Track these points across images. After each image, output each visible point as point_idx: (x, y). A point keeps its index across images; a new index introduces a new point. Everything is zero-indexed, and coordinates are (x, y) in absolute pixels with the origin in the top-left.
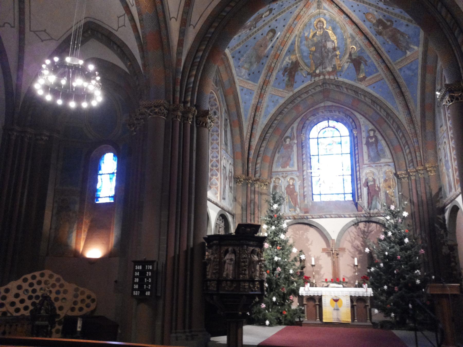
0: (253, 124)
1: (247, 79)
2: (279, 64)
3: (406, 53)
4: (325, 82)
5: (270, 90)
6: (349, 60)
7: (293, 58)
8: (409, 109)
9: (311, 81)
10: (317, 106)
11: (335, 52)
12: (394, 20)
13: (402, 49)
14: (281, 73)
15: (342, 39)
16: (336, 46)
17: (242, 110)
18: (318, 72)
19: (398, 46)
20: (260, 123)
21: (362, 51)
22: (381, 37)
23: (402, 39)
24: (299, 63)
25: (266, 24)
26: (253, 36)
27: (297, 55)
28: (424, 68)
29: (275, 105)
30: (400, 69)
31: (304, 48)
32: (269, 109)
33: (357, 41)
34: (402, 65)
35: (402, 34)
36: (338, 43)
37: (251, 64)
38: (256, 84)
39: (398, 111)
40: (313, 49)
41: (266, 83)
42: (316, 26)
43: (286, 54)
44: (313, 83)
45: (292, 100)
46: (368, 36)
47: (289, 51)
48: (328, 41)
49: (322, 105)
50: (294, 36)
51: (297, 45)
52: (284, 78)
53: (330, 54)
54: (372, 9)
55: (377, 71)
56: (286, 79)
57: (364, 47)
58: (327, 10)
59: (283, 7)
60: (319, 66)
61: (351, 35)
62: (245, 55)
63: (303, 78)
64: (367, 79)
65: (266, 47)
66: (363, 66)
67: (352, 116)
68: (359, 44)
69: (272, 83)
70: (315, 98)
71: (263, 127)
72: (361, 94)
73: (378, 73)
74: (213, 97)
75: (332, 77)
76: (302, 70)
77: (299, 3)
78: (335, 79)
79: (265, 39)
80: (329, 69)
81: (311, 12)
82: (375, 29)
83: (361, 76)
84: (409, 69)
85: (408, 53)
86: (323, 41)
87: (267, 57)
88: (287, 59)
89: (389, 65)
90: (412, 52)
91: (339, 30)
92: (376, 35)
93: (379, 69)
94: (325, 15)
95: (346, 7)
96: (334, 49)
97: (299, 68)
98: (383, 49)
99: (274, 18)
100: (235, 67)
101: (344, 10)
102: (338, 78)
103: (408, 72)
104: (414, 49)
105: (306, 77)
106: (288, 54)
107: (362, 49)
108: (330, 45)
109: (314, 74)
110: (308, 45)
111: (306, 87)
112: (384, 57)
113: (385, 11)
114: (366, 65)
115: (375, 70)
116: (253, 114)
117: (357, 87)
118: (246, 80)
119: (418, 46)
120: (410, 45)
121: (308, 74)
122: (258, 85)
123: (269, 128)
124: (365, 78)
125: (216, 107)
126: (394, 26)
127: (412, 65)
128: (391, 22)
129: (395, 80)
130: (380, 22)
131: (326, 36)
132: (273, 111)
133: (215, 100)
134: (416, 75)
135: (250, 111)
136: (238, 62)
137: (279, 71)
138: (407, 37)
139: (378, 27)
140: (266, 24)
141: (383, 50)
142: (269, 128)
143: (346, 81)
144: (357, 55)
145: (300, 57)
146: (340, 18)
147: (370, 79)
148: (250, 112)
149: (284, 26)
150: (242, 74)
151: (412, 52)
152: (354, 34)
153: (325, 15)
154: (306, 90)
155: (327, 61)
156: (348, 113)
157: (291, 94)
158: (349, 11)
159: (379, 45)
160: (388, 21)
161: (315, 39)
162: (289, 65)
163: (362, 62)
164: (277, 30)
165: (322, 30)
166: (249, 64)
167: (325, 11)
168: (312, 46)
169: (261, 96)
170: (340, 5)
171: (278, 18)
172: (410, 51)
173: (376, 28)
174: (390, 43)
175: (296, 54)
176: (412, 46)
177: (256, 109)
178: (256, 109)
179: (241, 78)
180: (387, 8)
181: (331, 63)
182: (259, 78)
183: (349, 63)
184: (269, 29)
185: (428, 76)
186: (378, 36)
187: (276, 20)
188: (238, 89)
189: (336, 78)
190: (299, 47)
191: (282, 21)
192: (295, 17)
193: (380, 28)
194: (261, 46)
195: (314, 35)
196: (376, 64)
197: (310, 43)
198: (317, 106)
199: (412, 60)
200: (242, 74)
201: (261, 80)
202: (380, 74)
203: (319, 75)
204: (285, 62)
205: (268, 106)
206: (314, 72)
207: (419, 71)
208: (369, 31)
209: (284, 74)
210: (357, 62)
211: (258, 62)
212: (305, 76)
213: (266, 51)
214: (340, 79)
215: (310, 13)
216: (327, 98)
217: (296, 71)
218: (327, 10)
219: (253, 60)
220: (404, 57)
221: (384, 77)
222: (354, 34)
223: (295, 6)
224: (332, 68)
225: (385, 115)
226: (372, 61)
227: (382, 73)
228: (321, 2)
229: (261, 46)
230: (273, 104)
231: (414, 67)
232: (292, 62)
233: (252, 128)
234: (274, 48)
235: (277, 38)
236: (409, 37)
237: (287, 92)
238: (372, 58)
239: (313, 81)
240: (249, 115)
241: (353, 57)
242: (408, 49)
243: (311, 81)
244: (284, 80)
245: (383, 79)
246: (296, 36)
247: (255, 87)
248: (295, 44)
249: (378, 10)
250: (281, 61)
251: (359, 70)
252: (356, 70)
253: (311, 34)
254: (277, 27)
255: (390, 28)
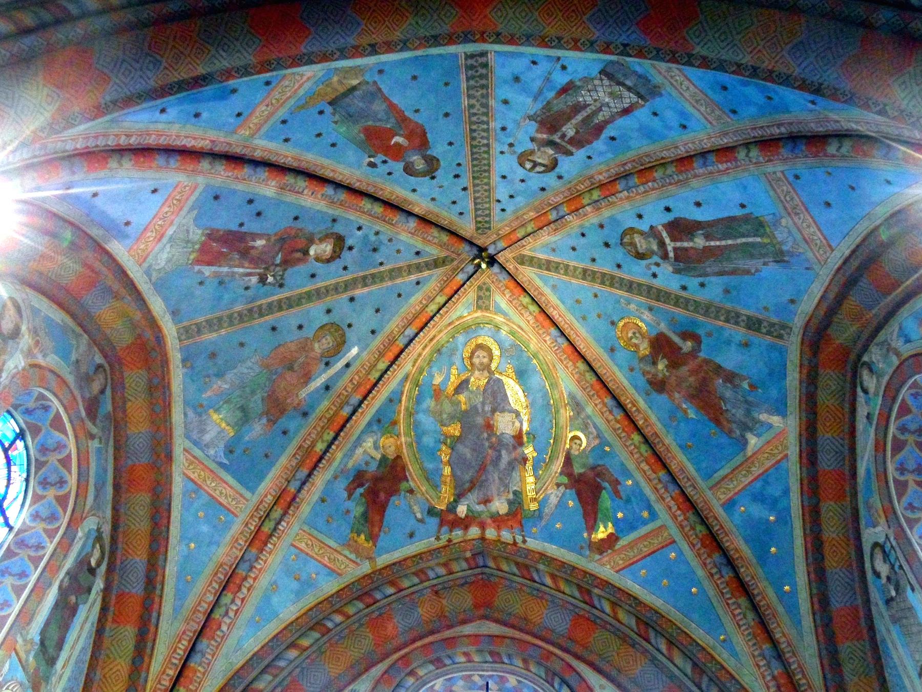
0: (200, 634)
1: (221, 465)
2: (339, 455)
3: (745, 443)
4: (483, 548)
5: (293, 529)
6: (565, 480)
7: (389, 445)
8: (774, 643)
9: (438, 539)
10: (448, 634)
11: (519, 450)
12: (701, 332)
13: (731, 431)
14: (341, 486)
15: (543, 406)
16: (525, 427)
17: (171, 570)
18: (462, 510)
19: (717, 422)
20: (231, 642)
21: (599, 449)
22: (663, 396)
23: (728, 394)
24: (404, 468)
25: (318, 294)
26: (269, 319)
27: (403, 439)
28: (812, 486)
29: (299, 594)
30: (730, 505)
31: (427, 421)
32: (275, 600)
33: (589, 417)
34: (734, 486)
35: (731, 378)
36: (530, 421)
37: (245, 416)
38: (248, 495)
39: (734, 654)
40: (455, 430)
41: (286, 501)
42: (471, 358)
43: (369, 424)
44: (444, 547)
45: (362, 591)
46: (622, 399)
47: (378, 420)
48: (503, 411)
49: (468, 629)
50: (400, 375)
51: (407, 409)
52: (350, 505)
53: (504, 452)
54: (639, 305)
55: (653, 516)
56: (357, 509)
57: (608, 435)
58: (505, 314)
59: (378, 257)
60: (470, 489)
61: (572, 397)
62: (229, 376)
63: (413, 522)
64: (622, 543)
65: (307, 378)
66: (606, 500)
67: (572, 679)
68: (595, 427)
69: (305, 510)
70: (444, 602)
71: (239, 661)
72: (599, 596)
73: (658, 523)
74: (60, 447)
75: (506, 536)
76: (411, 491)
77: (426, 273)
78: (515, 543)
79: (305, 346)
80: (500, 506)
81: (458, 314)
82: (644, 373)
83: (601, 533)
84: (759, 498)
85: (753, 441)
86: (488, 408)
87: (305, 414)
88: (369, 443)
89: (689, 491)
90: (767, 436)
91: (536, 381)
92: (648, 394)
93: (658, 507)
94: (497, 328)
95: (562, 307)
96: (518, 439)
97: (404, 485)
98: (669, 440)
99: (347, 286)
100: (186, 403)
101: (554, 314)
102: (524, 542)
103: (757, 511)
104: (770, 426)
105: (421, 521)
106: (375, 428)
107: (603, 442)
108: (505, 425)
109: (451, 517)
110: (441, 414)
111: (420, 556)
112: (674, 467)
113: (676, 301)
114: (617, 493)
115: (645, 514)
116: (210, 598)
117: (585, 573)
118: (213, 466)
119: (784, 415)
120: (756, 415)
121: (431, 512)
122: (255, 499)
123: (263, 672)
124: (611, 540)
125: (61, 493)
126: (702, 355)
127: (767, 483)
128: (696, 339)
129: (713, 541)
130: (661, 345)
131: (495, 396)
132: (288, 610)
133: (65, 462)
134: (784, 518)
135: (200, 586)
136: (200, 391)
137: (336, 477)
138: (745, 385)
139: (655, 363)
140: (318, 294)
141: (669, 441)
142: (263, 672)
143: (552, 550)
144: (591, 461)
145: (410, 445)
146: (540, 345)
147: (631, 546)
148: (201, 590)
149: (373, 332)
150: (207, 437)
151: (767, 436)
152: (580, 395)
153: (497, 328)
154: (416, 565)
155: (494, 476)
156: (557, 666)
157: (366, 568)
158: (570, 317)
159: (659, 427)
160: (685, 336)
161: (462, 398)
162: (373, 467)
163: (606, 485)
164: (351, 335)
165: (486, 373)
166: (239, 414)
167: (499, 319)
168: (452, 418)
169: (259, 540)
170: (542, 301)
171: (358, 292)
172: (758, 436)
173: (648, 369)
174: (692, 414)
175: (398, 436)
176: (763, 417)
177: (231, 581)
178: (231, 581)
179: (198, 452)
180: (684, 288)
181: (507, 486)
182: (261, 477)
183: (562, 489)
184: (326, 319)
185: (830, 510)
186: (654, 395)
187: (352, 299)
188: (178, 486)
189: (519, 539)
190: (410, 414)
191: (370, 311)
192: (410, 317)
193: (661, 366)
194: (291, 368)
195: (463, 386)
196: (648, 491)
197: (447, 407)
198: (448, 634)
199: (768, 464)
200: (207, 437)
201: (268, 485)
202: (663, 527)
203: (464, 523)
204: (359, 451)
205: (274, 586)
206: (452, 508)
207: (795, 501)
208: (626, 383)
209: (350, 492)
210: (588, 486)
211: (272, 422)
212: (419, 516)
213: (303, 393)
214: (533, 544)
215: (454, 317)
216: (484, 607)
217: (393, 491)
218: (505, 314)
219: (256, 403)
220: (739, 459)
221: (678, 537)
222: (580, 395)
223: (413, 277)
224: (510, 503)
225: (689, 670)
226: (636, 483)
227: (670, 523)
228: (488, 290)
229: (291, 368)
230: (295, 585)
231: (774, 491)
232: (384, 458)
233: (192, 651)
234: (333, 393)
235: (348, 365)
236: (752, 386)
237: (353, 556)
238: (638, 476)
239: (443, 542)
240: (190, 601)
241: (578, 469)
242: (751, 430)
243: (438, 539)
244: (348, 512)
245: (674, 542)
246: (406, 378)
247: (244, 503)
248: (400, 401)
249: (654, 303)
250: (349, 446)
251: (596, 513)
252: (586, 515)
253: (454, 380)
254: (350, 326)
255: (692, 365)
